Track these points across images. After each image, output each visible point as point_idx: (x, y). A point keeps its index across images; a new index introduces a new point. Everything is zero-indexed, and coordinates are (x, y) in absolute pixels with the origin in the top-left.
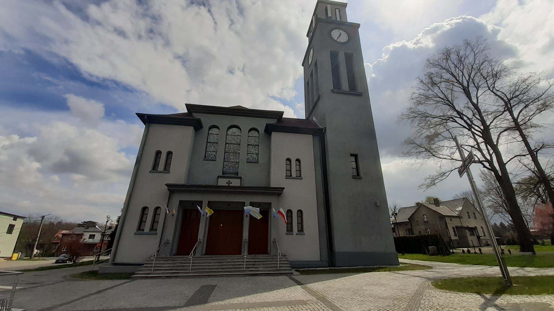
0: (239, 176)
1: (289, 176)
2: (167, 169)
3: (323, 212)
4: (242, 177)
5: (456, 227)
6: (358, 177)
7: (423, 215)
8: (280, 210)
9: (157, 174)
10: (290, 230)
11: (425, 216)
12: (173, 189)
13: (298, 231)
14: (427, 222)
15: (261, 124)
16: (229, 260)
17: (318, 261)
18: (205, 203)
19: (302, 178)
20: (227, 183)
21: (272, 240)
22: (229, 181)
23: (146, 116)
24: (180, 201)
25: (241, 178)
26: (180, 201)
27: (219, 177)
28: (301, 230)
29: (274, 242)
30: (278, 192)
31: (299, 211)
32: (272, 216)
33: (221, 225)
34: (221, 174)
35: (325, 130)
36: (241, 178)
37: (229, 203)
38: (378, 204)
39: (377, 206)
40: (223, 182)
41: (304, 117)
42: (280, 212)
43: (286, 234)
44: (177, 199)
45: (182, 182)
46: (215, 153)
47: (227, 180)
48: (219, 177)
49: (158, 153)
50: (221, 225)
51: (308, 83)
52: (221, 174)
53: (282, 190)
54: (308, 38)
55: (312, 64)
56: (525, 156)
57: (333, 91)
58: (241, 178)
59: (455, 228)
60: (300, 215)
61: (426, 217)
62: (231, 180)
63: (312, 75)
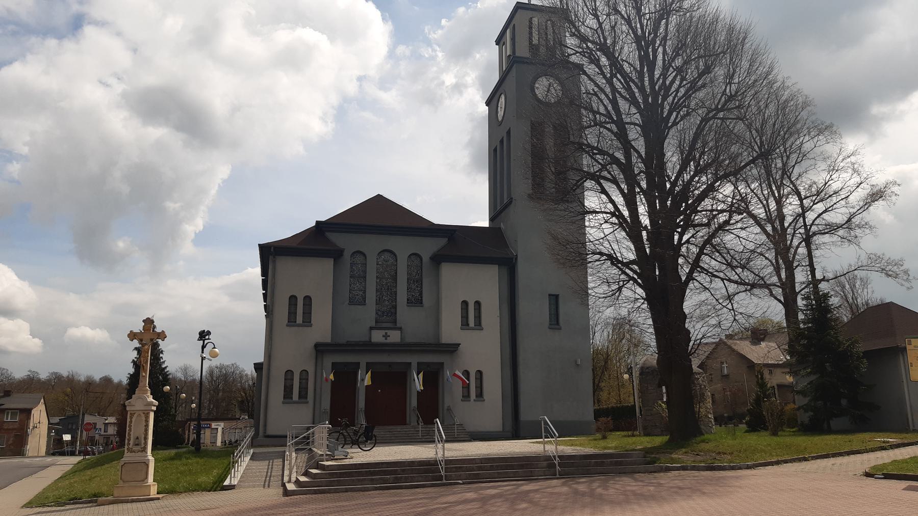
0: (398, 325)
1: (465, 324)
2: (307, 322)
3: (508, 372)
4: (403, 327)
5: (777, 385)
6: (557, 327)
7: (722, 363)
8: (456, 373)
9: (296, 328)
10: (466, 396)
11: (725, 365)
12: (320, 349)
13: (463, 396)
14: (727, 376)
15: (428, 247)
16: (399, 430)
17: (500, 432)
18: (363, 366)
19: (483, 328)
20: (383, 336)
21: (446, 407)
22: (386, 333)
23: (272, 248)
24: (332, 363)
25: (401, 328)
26: (332, 363)
27: (371, 328)
28: (480, 395)
29: (449, 409)
30: (452, 349)
31: (478, 372)
32: (445, 379)
33: (379, 391)
34: (373, 324)
35: (516, 259)
36: (400, 329)
37: (390, 364)
38: (579, 363)
39: (578, 365)
40: (377, 337)
41: (484, 222)
42: (455, 375)
43: (462, 400)
44: (329, 360)
45: (329, 340)
46: (361, 293)
47: (383, 332)
48: (371, 328)
49: (293, 299)
50: (379, 391)
51: (495, 150)
52: (373, 324)
53: (457, 346)
54: (497, 46)
55: (503, 123)
56: (828, 282)
57: (530, 196)
58: (400, 329)
59: (776, 387)
60: (478, 376)
61: (726, 367)
62: (389, 332)
63: (502, 142)
